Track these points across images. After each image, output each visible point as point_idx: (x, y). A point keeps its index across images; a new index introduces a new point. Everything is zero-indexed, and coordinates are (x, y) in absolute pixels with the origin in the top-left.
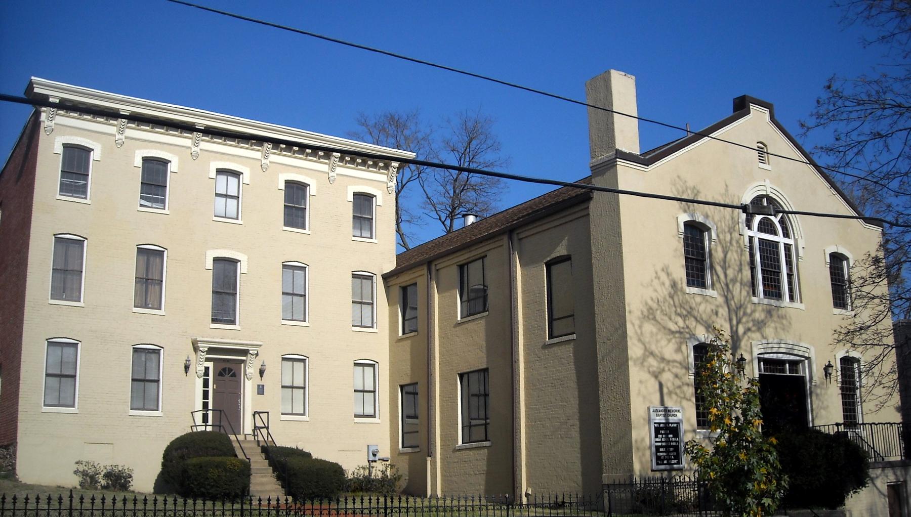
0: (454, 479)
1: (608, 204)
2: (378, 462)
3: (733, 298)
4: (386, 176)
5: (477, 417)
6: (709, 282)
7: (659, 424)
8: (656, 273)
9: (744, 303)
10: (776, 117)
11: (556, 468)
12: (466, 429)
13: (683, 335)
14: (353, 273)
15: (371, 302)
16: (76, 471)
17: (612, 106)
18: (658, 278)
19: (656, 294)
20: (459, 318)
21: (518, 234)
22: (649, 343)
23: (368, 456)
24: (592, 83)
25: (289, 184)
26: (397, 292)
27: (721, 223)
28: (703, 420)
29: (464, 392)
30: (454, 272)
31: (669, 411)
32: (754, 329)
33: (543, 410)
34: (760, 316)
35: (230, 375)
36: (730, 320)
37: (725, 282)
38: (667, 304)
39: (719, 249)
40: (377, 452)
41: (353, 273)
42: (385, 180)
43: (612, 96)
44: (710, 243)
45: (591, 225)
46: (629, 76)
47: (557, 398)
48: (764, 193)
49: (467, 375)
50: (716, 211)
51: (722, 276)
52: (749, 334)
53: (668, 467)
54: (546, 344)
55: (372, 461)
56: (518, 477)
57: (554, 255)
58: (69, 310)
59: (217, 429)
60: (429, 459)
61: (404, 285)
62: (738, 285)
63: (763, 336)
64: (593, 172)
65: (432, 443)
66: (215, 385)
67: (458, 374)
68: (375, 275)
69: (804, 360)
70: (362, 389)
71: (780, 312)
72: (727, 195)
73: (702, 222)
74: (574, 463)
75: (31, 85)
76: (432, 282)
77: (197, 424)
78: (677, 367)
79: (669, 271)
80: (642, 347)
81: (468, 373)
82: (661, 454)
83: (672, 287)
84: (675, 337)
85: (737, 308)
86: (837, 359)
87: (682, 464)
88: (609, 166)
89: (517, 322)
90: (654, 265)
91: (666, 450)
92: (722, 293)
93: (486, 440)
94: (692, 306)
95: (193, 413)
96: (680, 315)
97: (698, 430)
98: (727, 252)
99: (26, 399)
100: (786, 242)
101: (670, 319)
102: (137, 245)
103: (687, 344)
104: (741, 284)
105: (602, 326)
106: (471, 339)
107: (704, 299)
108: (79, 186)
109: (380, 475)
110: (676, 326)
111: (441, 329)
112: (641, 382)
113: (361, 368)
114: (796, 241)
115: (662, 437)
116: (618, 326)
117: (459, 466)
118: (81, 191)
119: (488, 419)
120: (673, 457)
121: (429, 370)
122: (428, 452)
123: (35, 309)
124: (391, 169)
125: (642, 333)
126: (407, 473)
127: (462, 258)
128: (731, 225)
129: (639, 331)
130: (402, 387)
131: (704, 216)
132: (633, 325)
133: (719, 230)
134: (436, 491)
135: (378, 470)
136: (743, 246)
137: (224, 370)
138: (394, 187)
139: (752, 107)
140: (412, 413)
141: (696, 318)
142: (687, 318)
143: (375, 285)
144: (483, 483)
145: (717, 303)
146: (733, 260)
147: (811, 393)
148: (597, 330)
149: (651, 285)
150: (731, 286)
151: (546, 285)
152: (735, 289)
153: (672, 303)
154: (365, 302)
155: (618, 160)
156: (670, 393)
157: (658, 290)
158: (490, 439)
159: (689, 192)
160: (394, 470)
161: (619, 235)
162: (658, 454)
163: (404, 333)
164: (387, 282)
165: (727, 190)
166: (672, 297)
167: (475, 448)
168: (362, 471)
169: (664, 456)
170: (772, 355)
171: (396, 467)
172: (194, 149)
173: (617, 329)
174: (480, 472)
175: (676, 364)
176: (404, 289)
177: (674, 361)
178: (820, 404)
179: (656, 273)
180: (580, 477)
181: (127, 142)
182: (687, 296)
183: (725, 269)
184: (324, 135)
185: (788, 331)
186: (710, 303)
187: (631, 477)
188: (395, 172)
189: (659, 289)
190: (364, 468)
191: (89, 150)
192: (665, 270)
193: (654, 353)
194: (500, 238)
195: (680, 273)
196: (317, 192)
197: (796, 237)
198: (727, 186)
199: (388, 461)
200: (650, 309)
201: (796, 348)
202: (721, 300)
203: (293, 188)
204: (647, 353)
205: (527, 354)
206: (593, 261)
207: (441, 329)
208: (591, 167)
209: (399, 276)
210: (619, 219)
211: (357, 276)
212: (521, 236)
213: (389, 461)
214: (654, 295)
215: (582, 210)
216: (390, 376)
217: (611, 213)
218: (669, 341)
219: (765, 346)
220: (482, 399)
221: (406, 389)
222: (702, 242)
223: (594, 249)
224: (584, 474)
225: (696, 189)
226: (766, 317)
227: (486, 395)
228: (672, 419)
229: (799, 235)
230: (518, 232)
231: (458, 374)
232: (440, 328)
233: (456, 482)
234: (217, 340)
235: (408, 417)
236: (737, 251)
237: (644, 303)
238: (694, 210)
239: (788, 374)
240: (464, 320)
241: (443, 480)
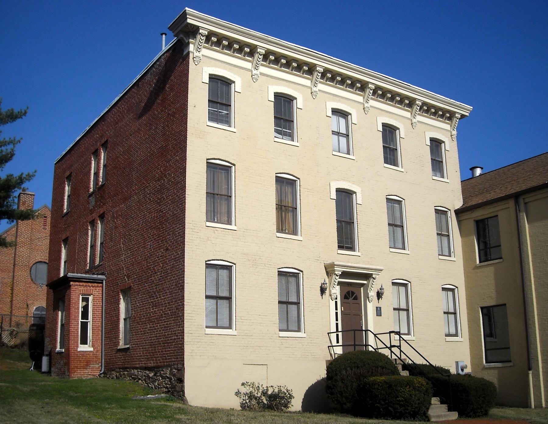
4: (410, 114)
15: (447, 234)
16: (237, 392)
25: (278, 96)
26: (472, 226)
35: (353, 298)
41: (277, 175)
42: (362, 101)
58: (223, 232)
59: (351, 349)
66: (343, 307)
75: (184, 15)
77: (333, 345)
95: (329, 334)
99: (190, 321)
102: (435, 207)
108: (222, 115)
118: (226, 120)
123: (194, 230)
124: (256, 56)
134: (541, 402)
137: (348, 293)
154: (444, 234)
163: (480, 262)
172: (255, 72)
181: (262, 78)
184: (411, 85)
188: (261, 60)
191: (291, 98)
196: (405, 135)
203: (218, 83)
209: (474, 211)
211: (224, 167)
234: (350, 264)
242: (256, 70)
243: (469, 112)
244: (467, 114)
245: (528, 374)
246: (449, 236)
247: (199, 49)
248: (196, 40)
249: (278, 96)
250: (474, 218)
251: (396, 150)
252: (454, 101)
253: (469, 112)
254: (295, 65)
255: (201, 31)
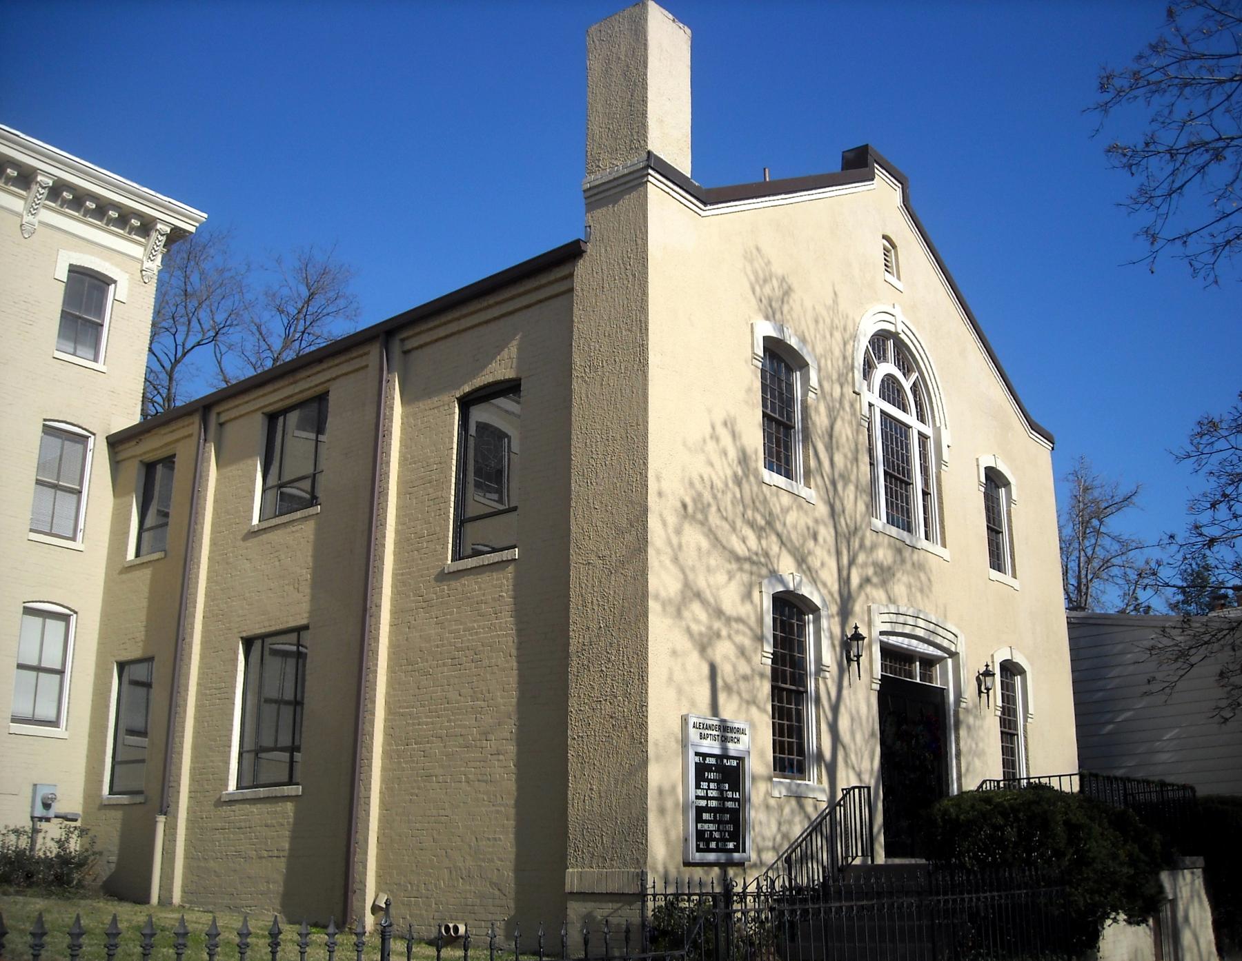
0: (212, 864)
1: (619, 264)
2: (54, 821)
3: (844, 511)
5: (272, 745)
6: (801, 470)
7: (704, 756)
8: (713, 428)
9: (861, 526)
10: (912, 203)
11: (449, 851)
12: (248, 758)
13: (759, 566)
14: (47, 423)
15: (78, 487)
17: (646, 67)
18: (715, 438)
19: (709, 469)
20: (255, 521)
21: (403, 340)
22: (693, 569)
23: (33, 807)
24: (602, 29)
25: (78, 274)
26: (133, 472)
27: (826, 360)
28: (793, 755)
29: (251, 676)
30: (257, 426)
31: (732, 730)
32: (875, 580)
33: (427, 717)
34: (885, 556)
36: (838, 554)
37: (831, 477)
38: (729, 496)
39: (822, 409)
40: (54, 799)
41: (47, 423)
43: (646, 49)
44: (805, 394)
45: (575, 310)
46: (681, 25)
47: (463, 691)
48: (891, 328)
49: (260, 641)
50: (818, 336)
51: (826, 464)
52: (869, 589)
53: (722, 857)
54: (446, 572)
55: (41, 819)
56: (358, 867)
57: (479, 382)
60: (161, 819)
61: (150, 458)
62: (851, 488)
63: (890, 598)
64: (589, 201)
65: (171, 784)
67: (242, 638)
68: (94, 434)
69: (946, 658)
70: (35, 663)
71: (915, 557)
72: (836, 311)
73: (796, 347)
74: (495, 839)
76: (207, 445)
78: (744, 634)
79: (737, 429)
80: (681, 576)
81: (263, 637)
82: (706, 826)
83: (740, 463)
84: (741, 569)
85: (849, 533)
86: (995, 663)
87: (744, 851)
88: (628, 186)
89: (384, 525)
90: (709, 411)
91: (715, 817)
92: (826, 497)
93: (290, 782)
94: (774, 510)
96: (752, 524)
97: (775, 779)
98: (835, 419)
100: (920, 430)
101: (734, 529)
103: (761, 587)
104: (857, 487)
105: (585, 526)
106: (277, 563)
107: (795, 500)
109: (54, 850)
110: (743, 546)
111: (215, 544)
112: (674, 653)
113: (39, 620)
114: (937, 431)
115: (709, 789)
116: (625, 524)
117: (224, 838)
119: (298, 749)
120: (727, 836)
121: (181, 628)
122: (161, 806)
124: (154, 235)
125: (680, 546)
126: (115, 849)
127: (274, 397)
128: (841, 368)
129: (675, 541)
130: (122, 666)
131: (799, 338)
132: (664, 523)
133: (822, 373)
134: (171, 891)
135: (48, 841)
136: (859, 416)
138: (156, 272)
139: (879, 171)
140: (138, 724)
141: (779, 535)
142: (764, 535)
143: (89, 455)
144: (280, 879)
145: (817, 514)
146: (844, 439)
147: (958, 724)
148: (573, 535)
149: (703, 451)
150: (840, 487)
151: (455, 446)
152: (846, 495)
153: (738, 495)
155: (650, 171)
156: (728, 688)
157: (715, 464)
158: (299, 780)
159: (775, 283)
160: (86, 839)
161: (640, 325)
162: (699, 825)
163: (138, 555)
164: (116, 453)
165: (835, 302)
166: (738, 483)
167: (264, 798)
168: (13, 837)
169: (711, 831)
170: (900, 639)
171: (91, 834)
173: (621, 532)
174: (270, 854)
175: (741, 627)
176: (149, 468)
177: (739, 620)
178: (974, 746)
179: (713, 428)
180: (509, 874)
182: (764, 487)
183: (830, 449)
184: (22, 135)
185: (928, 597)
186: (806, 513)
187: (642, 877)
188: (162, 243)
189: (715, 459)
190: (16, 832)
192: (729, 424)
193: (703, 595)
194: (361, 352)
195: (754, 438)
197: (938, 425)
198: (835, 294)
199: (76, 820)
200: (698, 498)
201: (940, 631)
202: (822, 510)
204: (689, 594)
205: (397, 593)
206: (575, 385)
207: (215, 544)
208: (584, 191)
209: (140, 440)
210: (645, 293)
212: (409, 345)
213: (80, 820)
214: (706, 471)
215: (556, 281)
216: (99, 644)
217: (626, 282)
218: (731, 575)
219: (894, 618)
220: (287, 712)
221: (129, 672)
222: (790, 387)
223: (577, 359)
224: (519, 869)
225: (787, 283)
226: (895, 562)
227: (297, 703)
228: (733, 748)
229: (943, 422)
230: (404, 335)
231: (242, 638)
232: (213, 543)
233: (215, 871)
235: (131, 732)
236: (851, 423)
237: (686, 481)
238: (783, 321)
239: (918, 681)
240: (266, 524)
241: (188, 868)
242: (32, 215)
243: (197, 225)
244: (193, 229)
245: (155, 823)
246: (80, 492)
247: (34, 209)
248: (149, 240)
249: (78, 274)
250: (141, 455)
251: (102, 325)
252: (152, 193)
253: (197, 225)
254: (91, 205)
255: (39, 178)
